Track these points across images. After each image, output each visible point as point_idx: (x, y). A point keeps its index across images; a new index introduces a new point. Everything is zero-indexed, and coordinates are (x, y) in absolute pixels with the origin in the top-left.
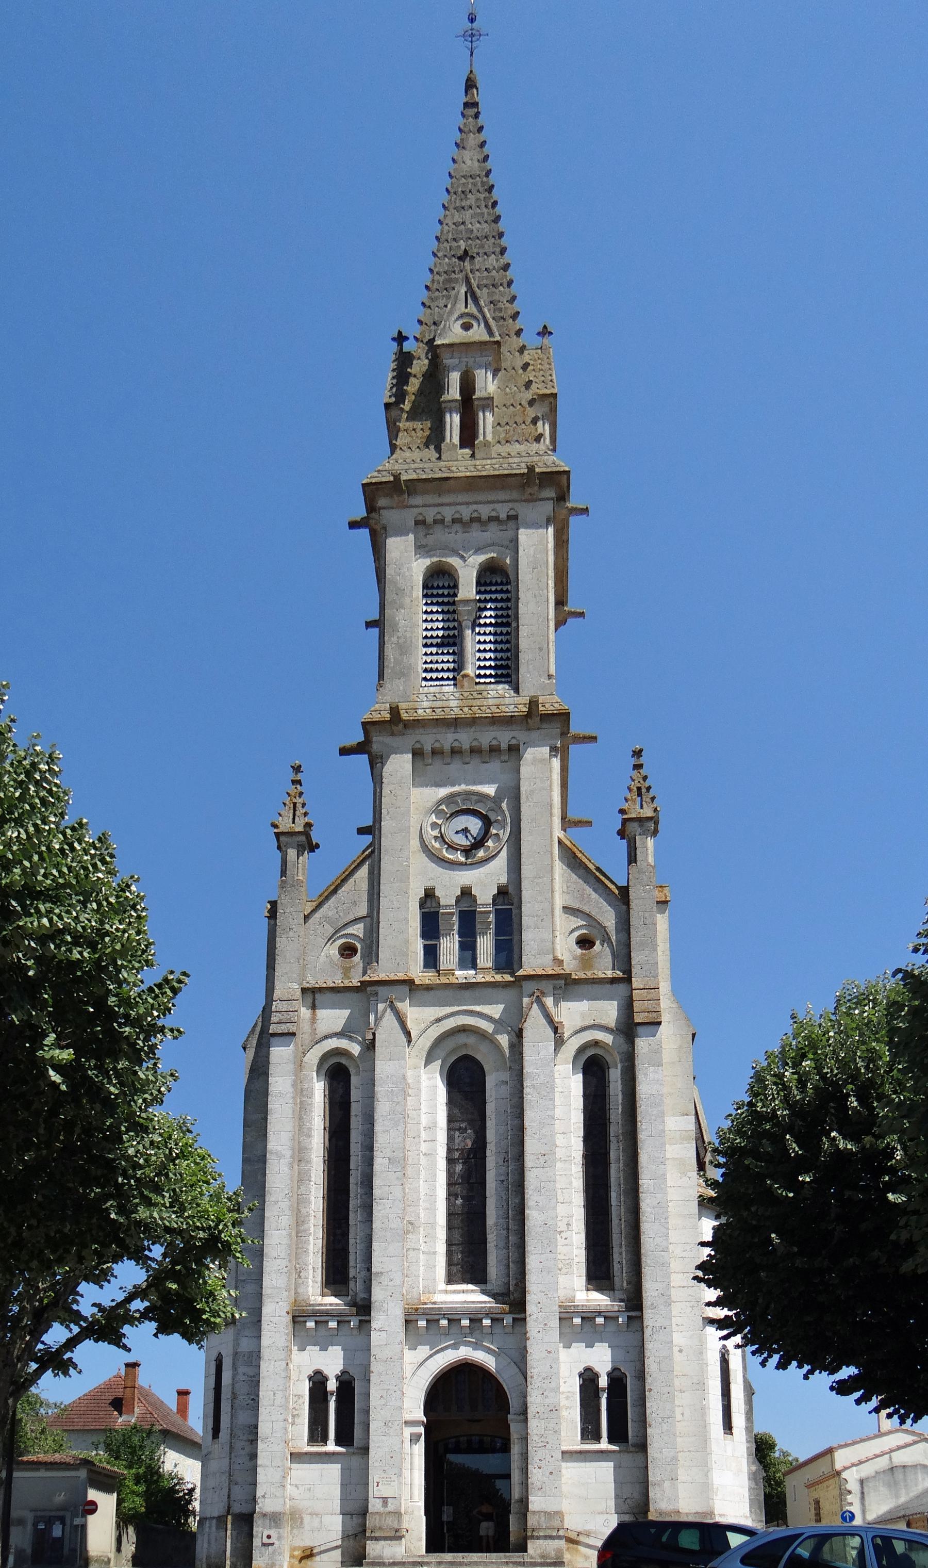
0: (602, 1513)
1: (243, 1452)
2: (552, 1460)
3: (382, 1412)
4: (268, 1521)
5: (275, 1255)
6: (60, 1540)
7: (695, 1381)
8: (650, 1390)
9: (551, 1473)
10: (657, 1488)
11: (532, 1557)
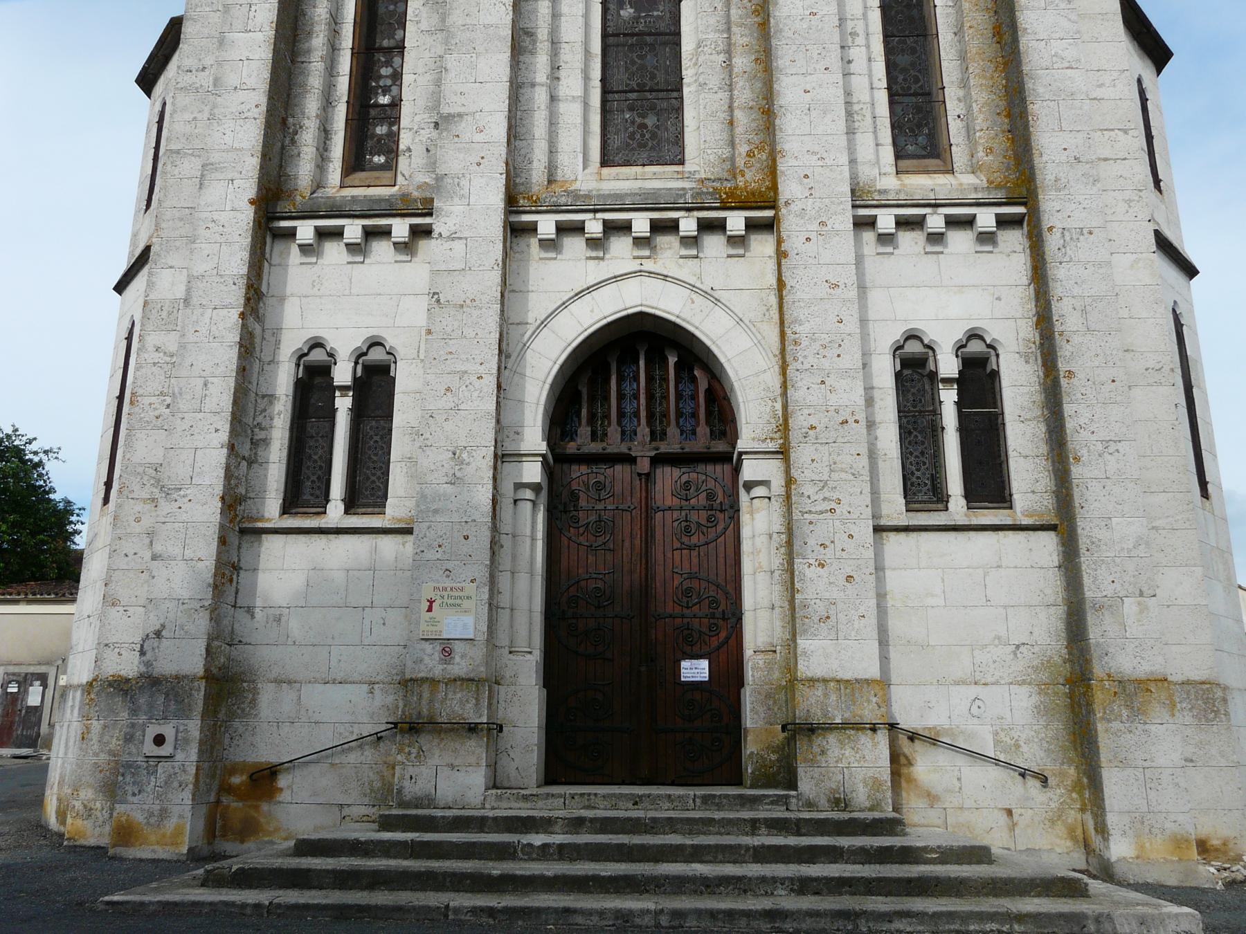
0: (964, 683)
1: (137, 528)
2: (850, 545)
3: (449, 426)
4: (161, 699)
5: (236, 83)
6: (37, 710)
7: (1151, 364)
8: (1070, 374)
9: (849, 578)
10: (1108, 618)
11: (810, 805)
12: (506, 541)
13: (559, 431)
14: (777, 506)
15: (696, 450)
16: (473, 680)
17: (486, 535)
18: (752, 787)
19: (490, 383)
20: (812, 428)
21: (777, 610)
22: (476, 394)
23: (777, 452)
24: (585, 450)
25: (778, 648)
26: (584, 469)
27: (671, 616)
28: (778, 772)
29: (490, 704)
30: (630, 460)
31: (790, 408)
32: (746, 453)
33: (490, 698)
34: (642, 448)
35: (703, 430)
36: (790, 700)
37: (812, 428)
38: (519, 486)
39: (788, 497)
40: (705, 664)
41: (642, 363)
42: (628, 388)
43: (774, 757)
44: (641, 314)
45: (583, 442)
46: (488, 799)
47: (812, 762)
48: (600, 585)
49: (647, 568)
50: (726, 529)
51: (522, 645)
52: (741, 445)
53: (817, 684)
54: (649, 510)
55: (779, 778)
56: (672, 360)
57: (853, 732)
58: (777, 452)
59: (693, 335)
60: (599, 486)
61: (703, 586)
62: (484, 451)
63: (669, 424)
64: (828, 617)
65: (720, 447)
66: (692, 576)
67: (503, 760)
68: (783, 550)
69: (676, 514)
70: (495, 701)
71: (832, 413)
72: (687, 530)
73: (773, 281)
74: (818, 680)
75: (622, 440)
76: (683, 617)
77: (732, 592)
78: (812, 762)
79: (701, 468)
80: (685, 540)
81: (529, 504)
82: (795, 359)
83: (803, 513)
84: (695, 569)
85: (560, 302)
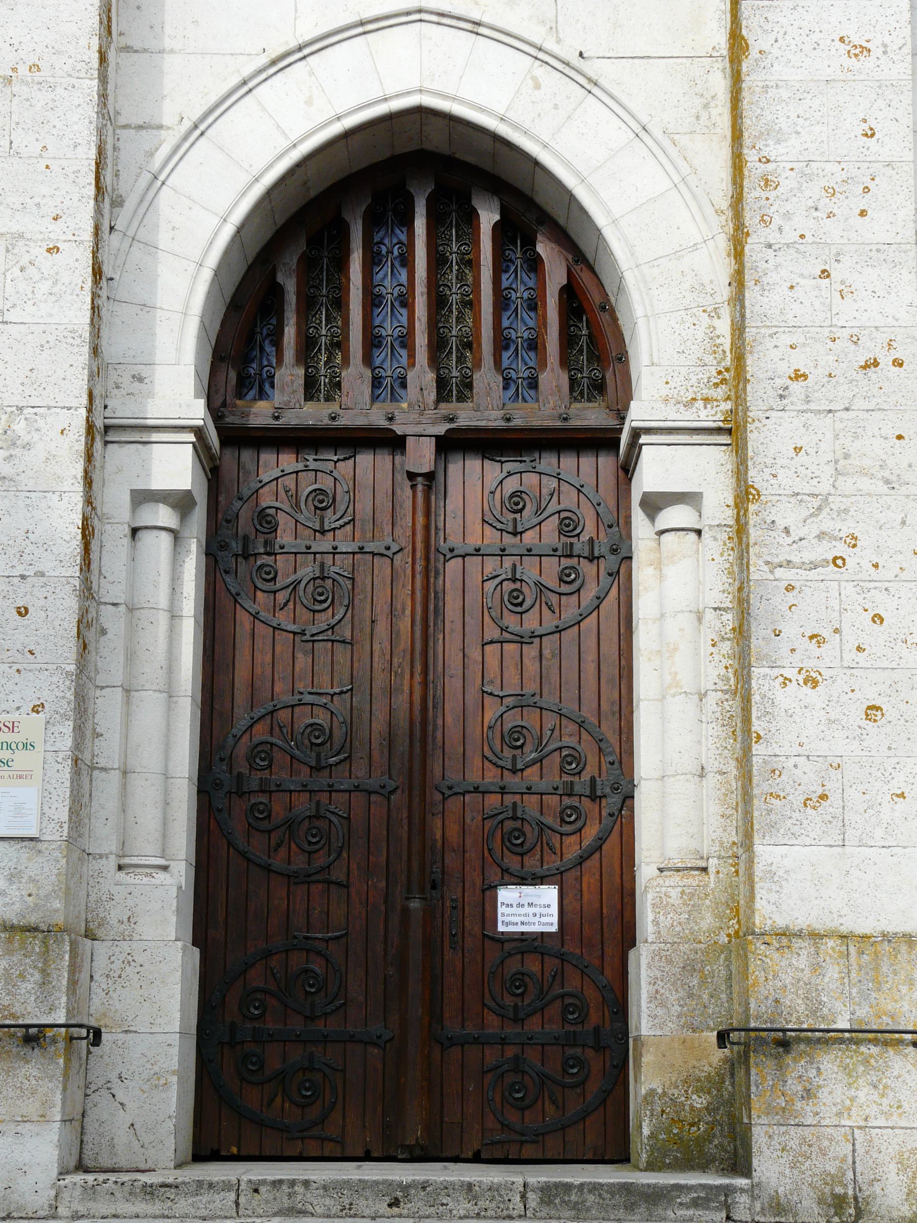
12: (113, 621)
13: (233, 375)
14: (715, 547)
15: (536, 423)
16: (36, 929)
17: (66, 607)
18: (651, 1167)
19: (77, 263)
20: (798, 376)
21: (712, 780)
22: (44, 287)
23: (719, 431)
24: (291, 419)
25: (713, 864)
26: (288, 461)
27: (476, 790)
28: (709, 1137)
29: (73, 983)
30: (391, 442)
31: (750, 333)
32: (649, 431)
33: (74, 968)
34: (418, 416)
35: (553, 378)
36: (737, 977)
37: (798, 376)
38: (143, 497)
39: (741, 529)
40: (549, 895)
41: (420, 225)
42: (389, 282)
43: (699, 1102)
44: (420, 111)
45: (285, 400)
46: (66, 1195)
47: (785, 1115)
48: (322, 718)
49: (425, 684)
50: (600, 599)
51: (146, 850)
52: (640, 413)
53: (797, 943)
54: (430, 555)
55: (711, 1149)
56: (488, 217)
57: (874, 1050)
58: (719, 431)
59: (536, 163)
60: (322, 501)
61: (548, 725)
62: (62, 419)
63: (478, 364)
64: (824, 797)
65: (591, 415)
66: (522, 703)
67: (102, 1109)
68: (726, 647)
69: (491, 565)
70: (84, 976)
71: (843, 344)
72: (516, 601)
73: (720, 39)
74: (799, 935)
75: (375, 398)
76: (503, 791)
77: (613, 738)
78: (785, 1115)
79: (548, 462)
80: (511, 621)
81: (165, 539)
82: (765, 221)
83: (773, 566)
84: (531, 687)
85: (235, 80)
